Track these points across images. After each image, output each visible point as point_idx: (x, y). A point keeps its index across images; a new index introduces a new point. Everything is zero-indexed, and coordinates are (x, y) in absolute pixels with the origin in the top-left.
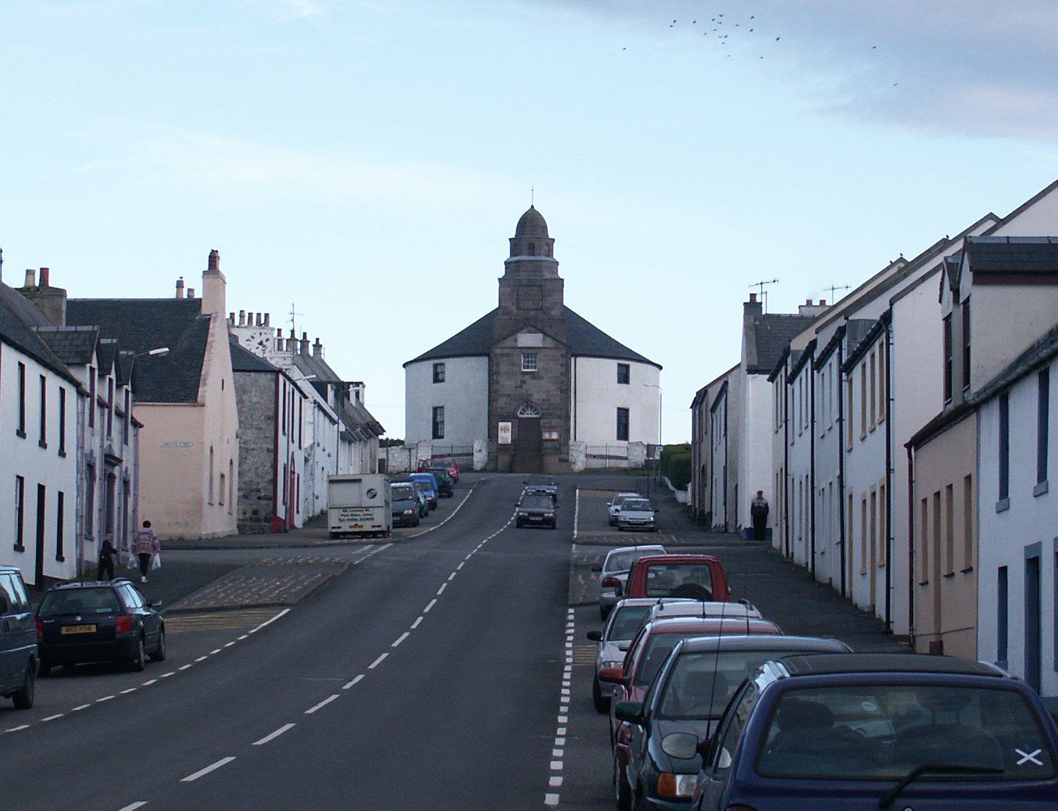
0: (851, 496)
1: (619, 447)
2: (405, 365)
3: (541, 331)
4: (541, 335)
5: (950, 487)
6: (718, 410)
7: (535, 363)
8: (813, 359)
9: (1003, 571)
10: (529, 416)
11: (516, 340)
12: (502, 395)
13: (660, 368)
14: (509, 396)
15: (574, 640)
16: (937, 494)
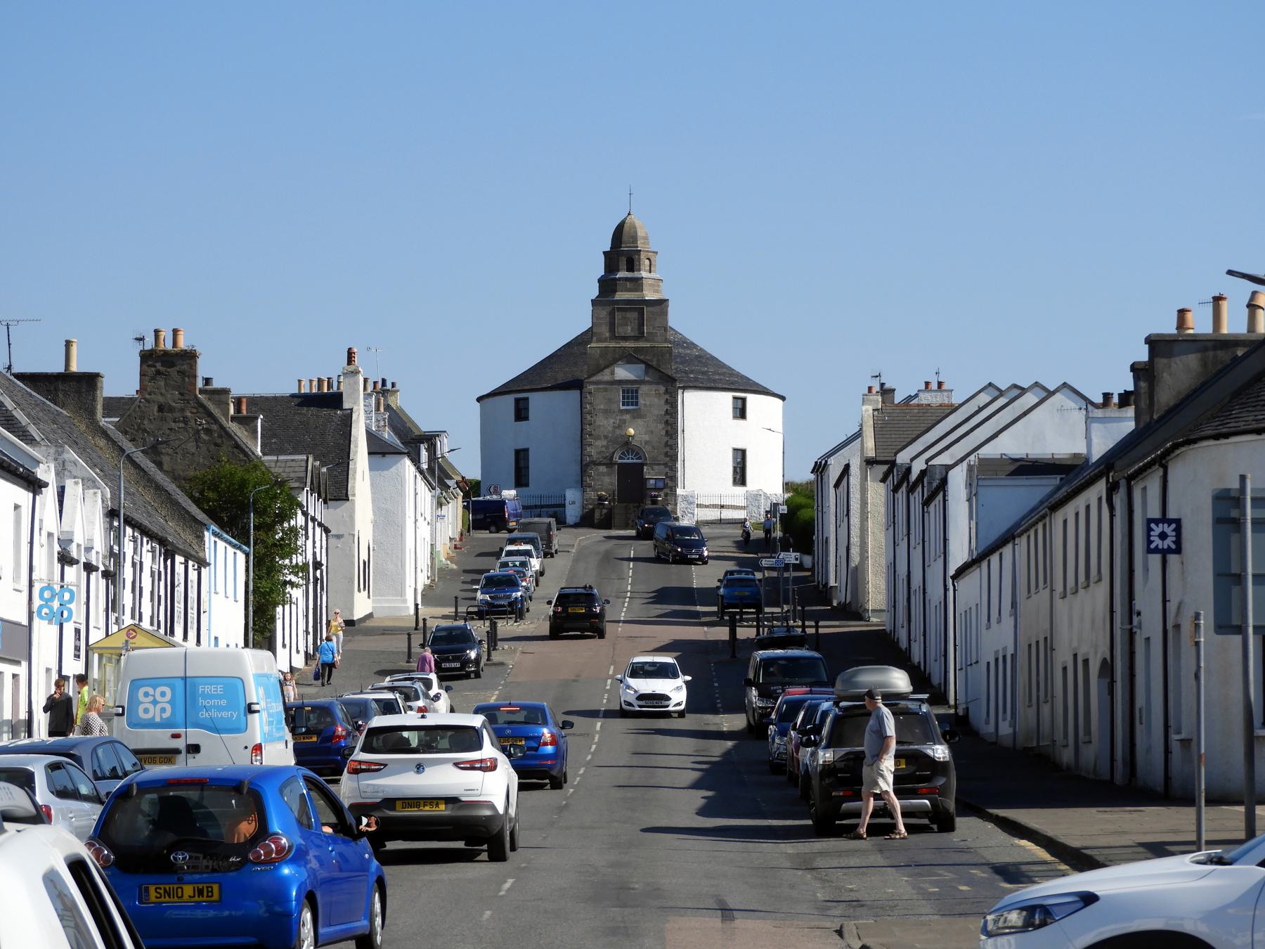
0: (930, 600)
1: (737, 495)
2: (479, 400)
3: (642, 362)
4: (643, 366)
5: (970, 608)
6: (841, 486)
7: (637, 398)
8: (908, 483)
9: (988, 663)
10: (630, 461)
11: (613, 373)
12: (598, 438)
13: (894, 390)
14: (606, 437)
15: (716, 705)
16: (966, 611)
